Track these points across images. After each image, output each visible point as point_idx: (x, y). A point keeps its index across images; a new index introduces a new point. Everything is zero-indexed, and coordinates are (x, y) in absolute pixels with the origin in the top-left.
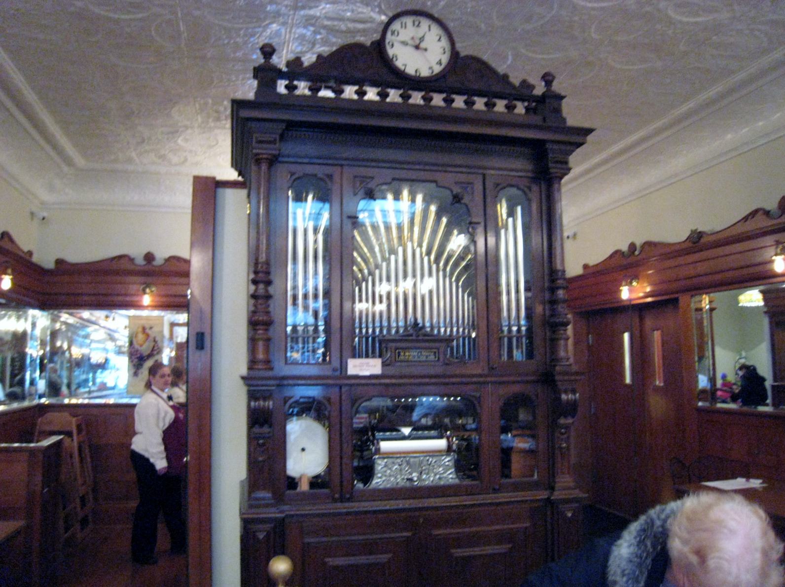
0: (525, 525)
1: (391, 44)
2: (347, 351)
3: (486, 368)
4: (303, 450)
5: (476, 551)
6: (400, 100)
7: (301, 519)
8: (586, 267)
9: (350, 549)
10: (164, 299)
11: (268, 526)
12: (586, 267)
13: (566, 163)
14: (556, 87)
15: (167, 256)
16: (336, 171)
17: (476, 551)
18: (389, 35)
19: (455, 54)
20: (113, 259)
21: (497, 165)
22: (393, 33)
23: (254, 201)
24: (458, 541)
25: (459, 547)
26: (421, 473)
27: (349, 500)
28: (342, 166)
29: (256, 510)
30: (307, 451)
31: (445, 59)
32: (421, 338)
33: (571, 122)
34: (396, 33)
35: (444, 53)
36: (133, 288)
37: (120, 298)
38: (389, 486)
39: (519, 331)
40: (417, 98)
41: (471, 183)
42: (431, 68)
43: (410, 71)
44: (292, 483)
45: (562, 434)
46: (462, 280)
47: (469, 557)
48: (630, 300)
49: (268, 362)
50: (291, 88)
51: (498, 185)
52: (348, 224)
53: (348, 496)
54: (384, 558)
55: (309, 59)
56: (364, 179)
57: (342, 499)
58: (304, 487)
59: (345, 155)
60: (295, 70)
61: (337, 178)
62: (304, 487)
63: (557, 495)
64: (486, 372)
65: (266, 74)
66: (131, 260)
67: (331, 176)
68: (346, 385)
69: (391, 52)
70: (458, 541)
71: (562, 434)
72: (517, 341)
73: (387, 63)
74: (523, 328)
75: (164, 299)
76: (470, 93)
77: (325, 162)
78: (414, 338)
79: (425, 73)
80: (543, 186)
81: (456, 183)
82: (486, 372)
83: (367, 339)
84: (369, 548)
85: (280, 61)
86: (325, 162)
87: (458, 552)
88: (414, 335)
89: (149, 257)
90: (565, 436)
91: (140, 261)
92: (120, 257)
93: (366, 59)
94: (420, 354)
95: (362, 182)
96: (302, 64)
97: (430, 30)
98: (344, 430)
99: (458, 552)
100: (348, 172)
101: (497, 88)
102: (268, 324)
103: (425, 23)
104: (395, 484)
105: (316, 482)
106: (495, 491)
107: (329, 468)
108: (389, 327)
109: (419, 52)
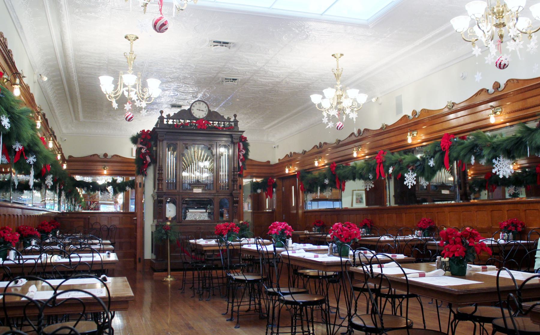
2: (181, 170)
8: (279, 160)
10: (112, 172)
12: (279, 160)
14: (237, 118)
15: (113, 154)
18: (192, 108)
19: (209, 111)
20: (91, 156)
23: (181, 177)
30: (171, 211)
33: (240, 130)
36: (100, 167)
37: (94, 171)
48: (289, 173)
49: (162, 189)
50: (167, 121)
52: (181, 156)
55: (172, 115)
56: (185, 144)
60: (169, 117)
61: (179, 144)
66: (98, 156)
69: (192, 112)
73: (192, 115)
75: (112, 172)
89: (106, 155)
91: (102, 156)
92: (94, 155)
102: (162, 180)
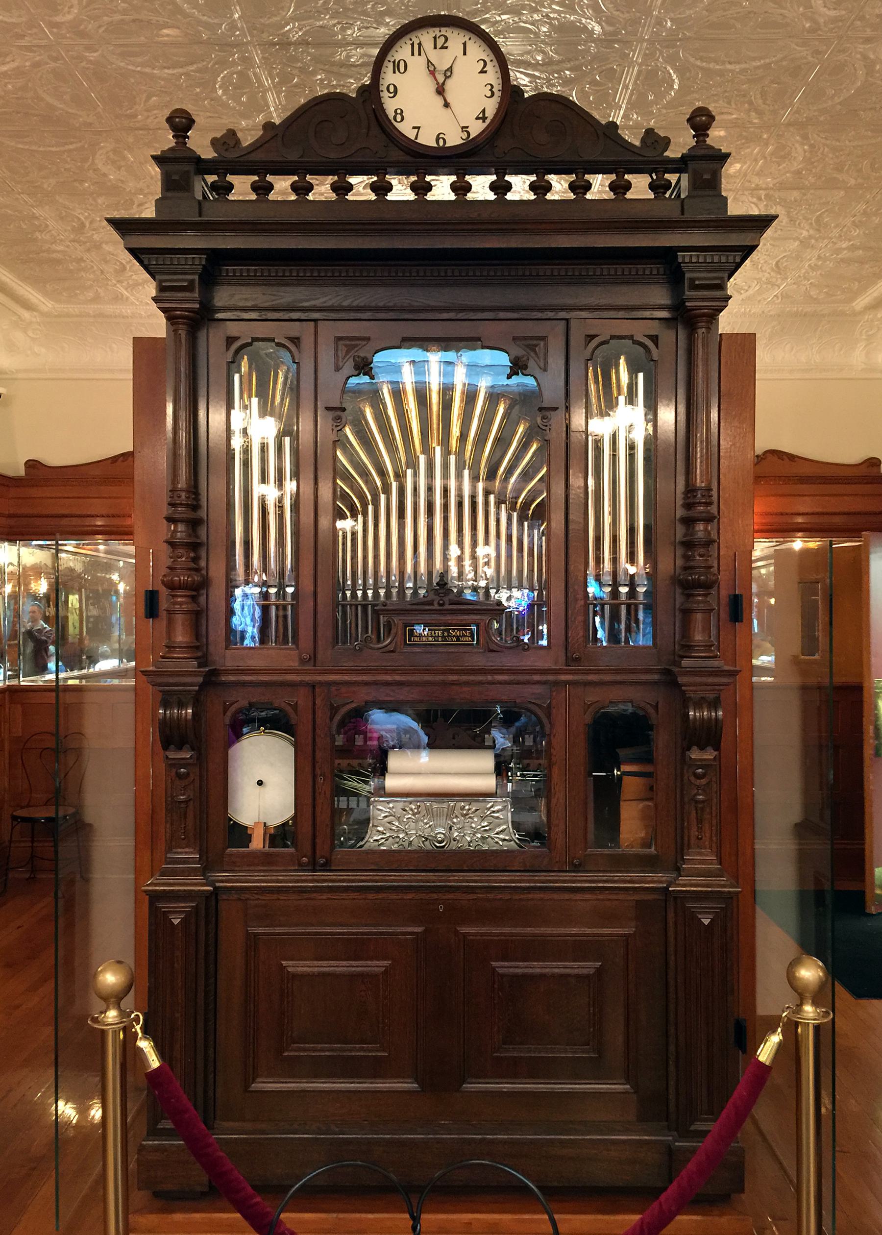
0: (626, 931)
1: (392, 89)
3: (562, 659)
4: (260, 783)
5: (536, 967)
6: (410, 196)
7: (244, 896)
9: (326, 948)
11: (187, 906)
13: (722, 287)
16: (305, 331)
17: (536, 967)
18: (389, 77)
19: (510, 93)
21: (592, 301)
22: (396, 67)
24: (510, 949)
25: (504, 959)
26: (450, 828)
27: (326, 867)
28: (315, 321)
29: (171, 879)
31: (491, 107)
32: (447, 607)
34: (402, 64)
35: (493, 94)
38: (395, 847)
39: (632, 593)
40: (442, 188)
41: (543, 338)
42: (464, 128)
43: (427, 139)
44: (239, 834)
45: (698, 777)
46: (358, 505)
47: (524, 976)
51: (591, 337)
53: (322, 861)
54: (377, 966)
57: (314, 866)
58: (257, 843)
59: (317, 303)
60: (231, 158)
61: (307, 342)
62: (257, 843)
63: (685, 884)
64: (561, 666)
65: (178, 167)
67: (298, 338)
68: (321, 683)
69: (390, 106)
70: (510, 949)
71: (698, 777)
72: (628, 612)
74: (641, 590)
76: (539, 168)
77: (287, 316)
78: (436, 607)
79: (454, 139)
80: (682, 335)
81: (515, 339)
82: (561, 666)
83: (365, 607)
84: (356, 948)
85: (200, 144)
86: (287, 316)
87: (503, 967)
88: (435, 603)
90: (703, 781)
93: (348, 127)
94: (446, 634)
95: (350, 349)
96: (238, 142)
97: (465, 54)
98: (319, 754)
99: (503, 967)
100: (329, 331)
101: (591, 155)
103: (456, 38)
104: (406, 844)
105: (280, 835)
106: (576, 868)
107: (294, 818)
108: (402, 588)
109: (440, 99)
